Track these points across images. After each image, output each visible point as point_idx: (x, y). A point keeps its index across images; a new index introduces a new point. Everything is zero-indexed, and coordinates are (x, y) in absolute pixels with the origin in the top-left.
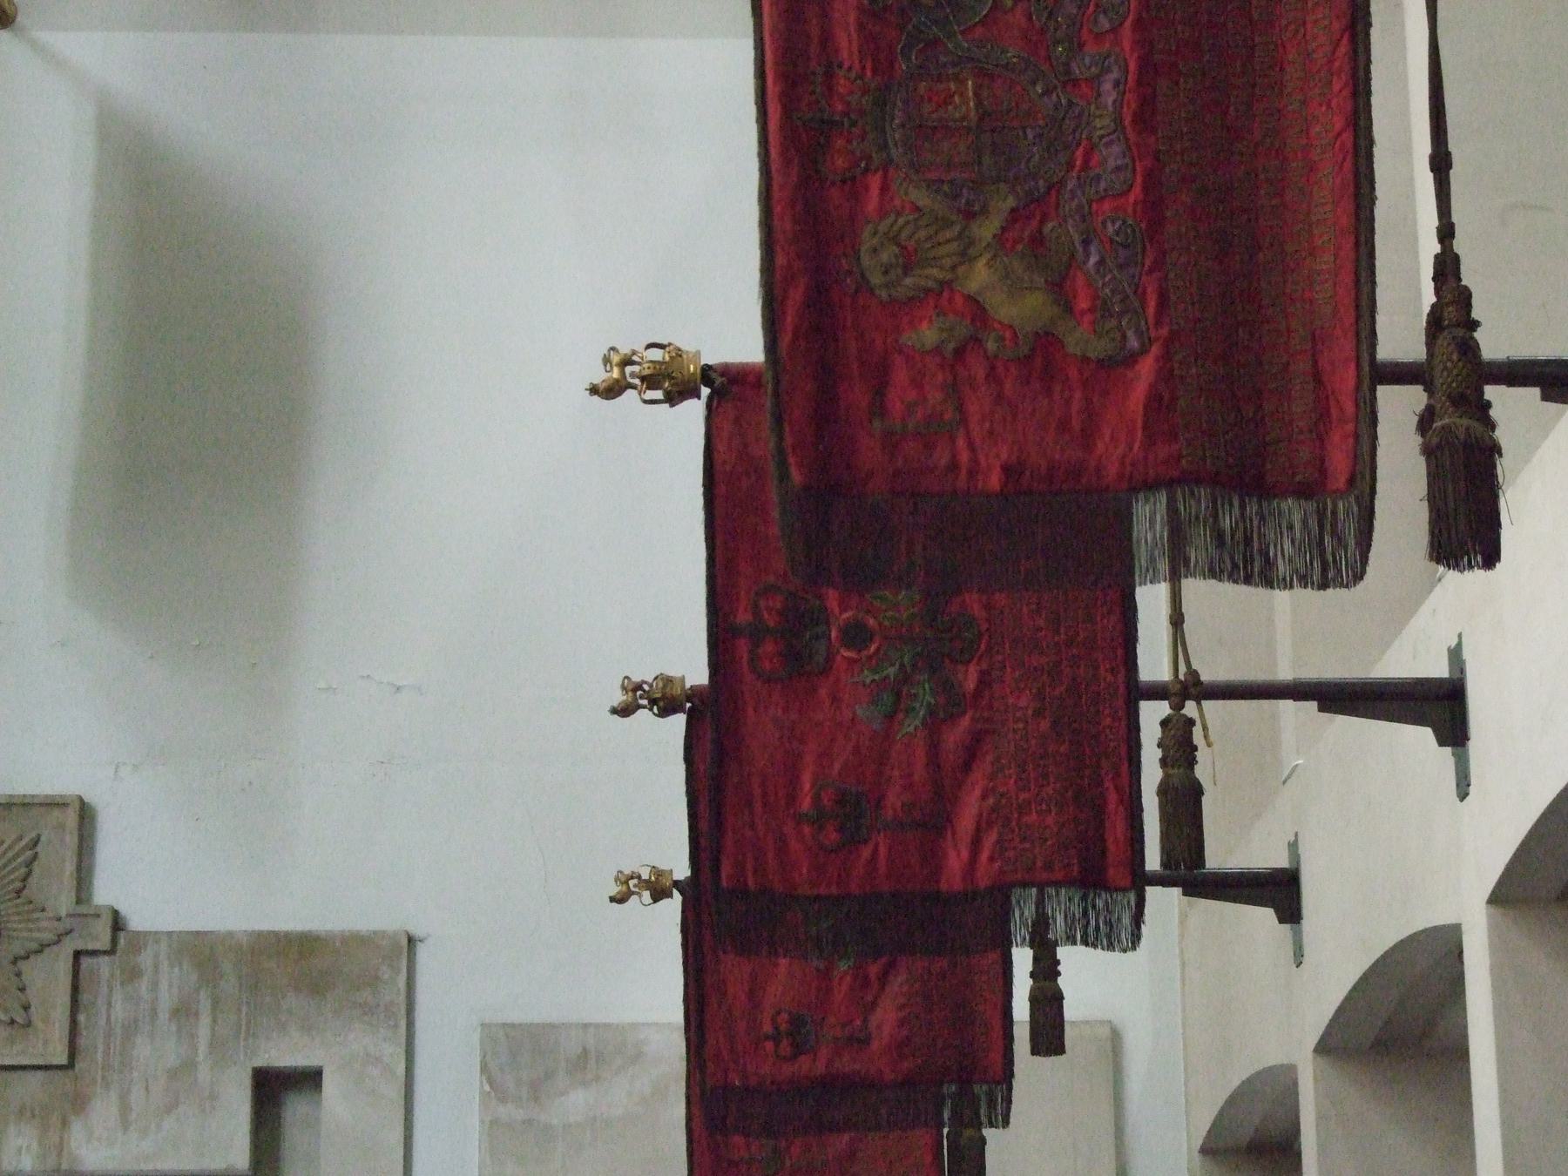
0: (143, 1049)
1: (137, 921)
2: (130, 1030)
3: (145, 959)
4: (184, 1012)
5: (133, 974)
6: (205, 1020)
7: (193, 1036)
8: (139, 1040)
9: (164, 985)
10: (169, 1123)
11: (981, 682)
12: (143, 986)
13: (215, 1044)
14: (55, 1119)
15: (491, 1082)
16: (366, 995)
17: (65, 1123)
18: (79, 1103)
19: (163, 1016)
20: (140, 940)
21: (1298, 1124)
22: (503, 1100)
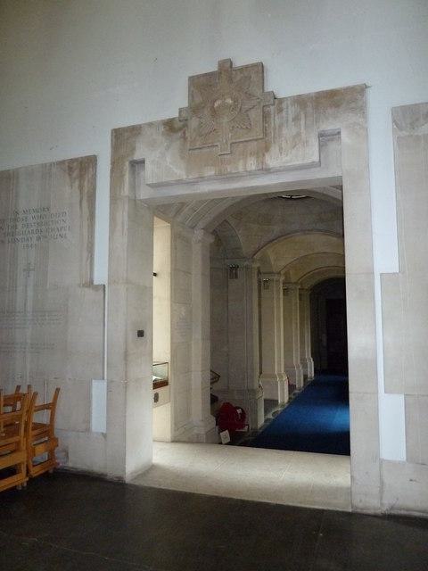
0: (285, 131)
1: (281, 95)
2: (281, 126)
3: (284, 105)
4: (296, 119)
5: (280, 110)
6: (303, 122)
7: (300, 125)
8: (284, 129)
9: (290, 112)
10: (294, 152)
11: (81, 163)
12: (284, 113)
13: (306, 127)
14: (261, 154)
15: (396, 124)
16: (353, 105)
17: (264, 155)
18: (267, 149)
19: (290, 119)
20: (281, 101)
21: (343, 256)
22: (401, 130)
